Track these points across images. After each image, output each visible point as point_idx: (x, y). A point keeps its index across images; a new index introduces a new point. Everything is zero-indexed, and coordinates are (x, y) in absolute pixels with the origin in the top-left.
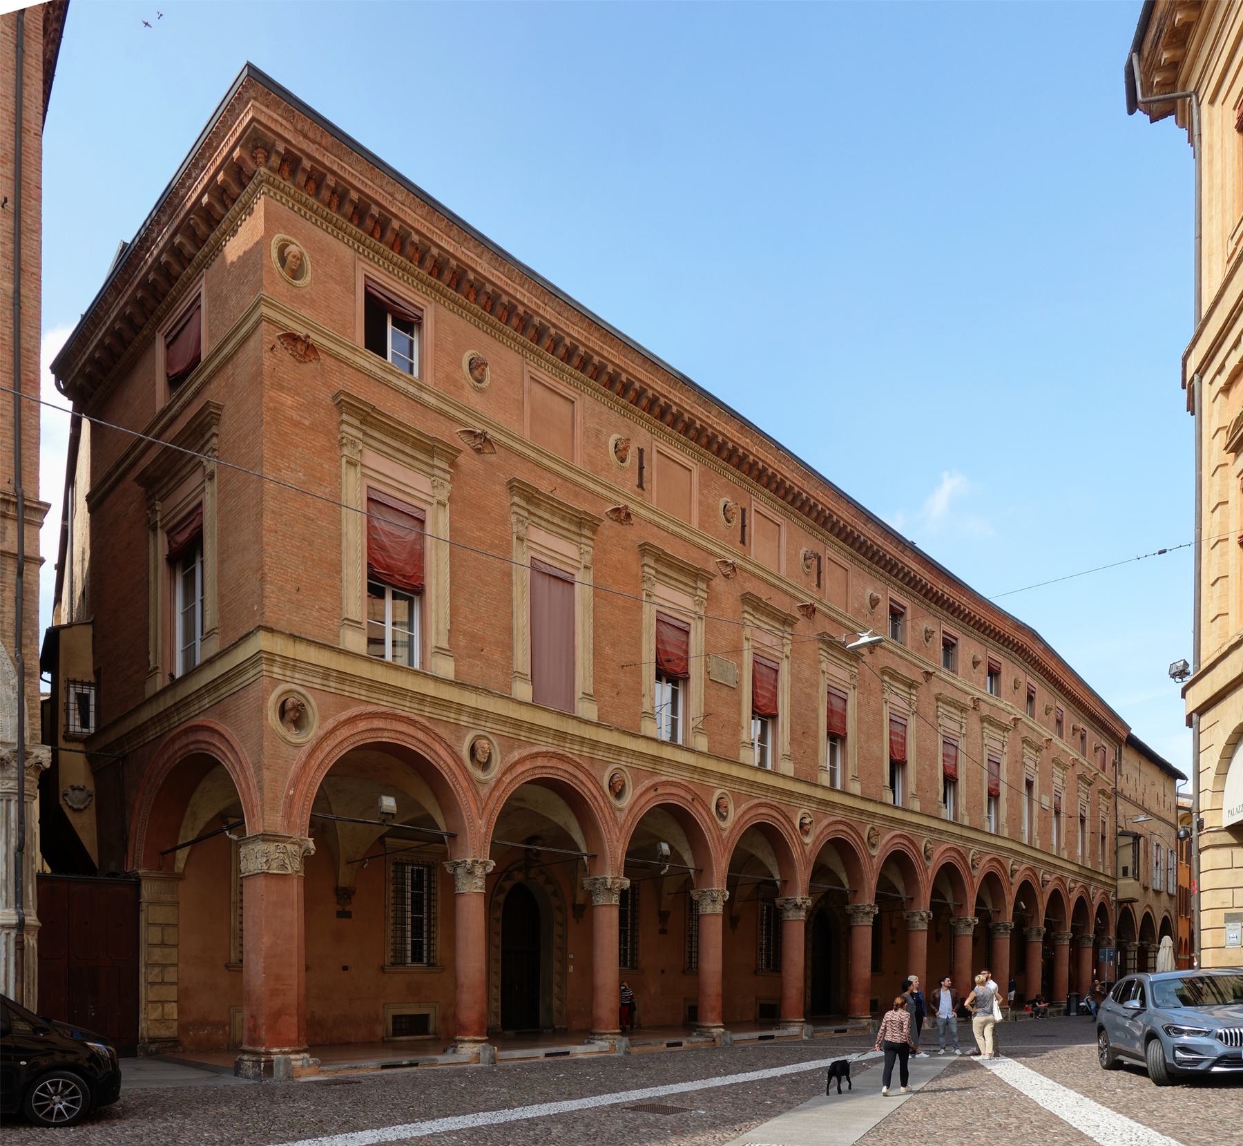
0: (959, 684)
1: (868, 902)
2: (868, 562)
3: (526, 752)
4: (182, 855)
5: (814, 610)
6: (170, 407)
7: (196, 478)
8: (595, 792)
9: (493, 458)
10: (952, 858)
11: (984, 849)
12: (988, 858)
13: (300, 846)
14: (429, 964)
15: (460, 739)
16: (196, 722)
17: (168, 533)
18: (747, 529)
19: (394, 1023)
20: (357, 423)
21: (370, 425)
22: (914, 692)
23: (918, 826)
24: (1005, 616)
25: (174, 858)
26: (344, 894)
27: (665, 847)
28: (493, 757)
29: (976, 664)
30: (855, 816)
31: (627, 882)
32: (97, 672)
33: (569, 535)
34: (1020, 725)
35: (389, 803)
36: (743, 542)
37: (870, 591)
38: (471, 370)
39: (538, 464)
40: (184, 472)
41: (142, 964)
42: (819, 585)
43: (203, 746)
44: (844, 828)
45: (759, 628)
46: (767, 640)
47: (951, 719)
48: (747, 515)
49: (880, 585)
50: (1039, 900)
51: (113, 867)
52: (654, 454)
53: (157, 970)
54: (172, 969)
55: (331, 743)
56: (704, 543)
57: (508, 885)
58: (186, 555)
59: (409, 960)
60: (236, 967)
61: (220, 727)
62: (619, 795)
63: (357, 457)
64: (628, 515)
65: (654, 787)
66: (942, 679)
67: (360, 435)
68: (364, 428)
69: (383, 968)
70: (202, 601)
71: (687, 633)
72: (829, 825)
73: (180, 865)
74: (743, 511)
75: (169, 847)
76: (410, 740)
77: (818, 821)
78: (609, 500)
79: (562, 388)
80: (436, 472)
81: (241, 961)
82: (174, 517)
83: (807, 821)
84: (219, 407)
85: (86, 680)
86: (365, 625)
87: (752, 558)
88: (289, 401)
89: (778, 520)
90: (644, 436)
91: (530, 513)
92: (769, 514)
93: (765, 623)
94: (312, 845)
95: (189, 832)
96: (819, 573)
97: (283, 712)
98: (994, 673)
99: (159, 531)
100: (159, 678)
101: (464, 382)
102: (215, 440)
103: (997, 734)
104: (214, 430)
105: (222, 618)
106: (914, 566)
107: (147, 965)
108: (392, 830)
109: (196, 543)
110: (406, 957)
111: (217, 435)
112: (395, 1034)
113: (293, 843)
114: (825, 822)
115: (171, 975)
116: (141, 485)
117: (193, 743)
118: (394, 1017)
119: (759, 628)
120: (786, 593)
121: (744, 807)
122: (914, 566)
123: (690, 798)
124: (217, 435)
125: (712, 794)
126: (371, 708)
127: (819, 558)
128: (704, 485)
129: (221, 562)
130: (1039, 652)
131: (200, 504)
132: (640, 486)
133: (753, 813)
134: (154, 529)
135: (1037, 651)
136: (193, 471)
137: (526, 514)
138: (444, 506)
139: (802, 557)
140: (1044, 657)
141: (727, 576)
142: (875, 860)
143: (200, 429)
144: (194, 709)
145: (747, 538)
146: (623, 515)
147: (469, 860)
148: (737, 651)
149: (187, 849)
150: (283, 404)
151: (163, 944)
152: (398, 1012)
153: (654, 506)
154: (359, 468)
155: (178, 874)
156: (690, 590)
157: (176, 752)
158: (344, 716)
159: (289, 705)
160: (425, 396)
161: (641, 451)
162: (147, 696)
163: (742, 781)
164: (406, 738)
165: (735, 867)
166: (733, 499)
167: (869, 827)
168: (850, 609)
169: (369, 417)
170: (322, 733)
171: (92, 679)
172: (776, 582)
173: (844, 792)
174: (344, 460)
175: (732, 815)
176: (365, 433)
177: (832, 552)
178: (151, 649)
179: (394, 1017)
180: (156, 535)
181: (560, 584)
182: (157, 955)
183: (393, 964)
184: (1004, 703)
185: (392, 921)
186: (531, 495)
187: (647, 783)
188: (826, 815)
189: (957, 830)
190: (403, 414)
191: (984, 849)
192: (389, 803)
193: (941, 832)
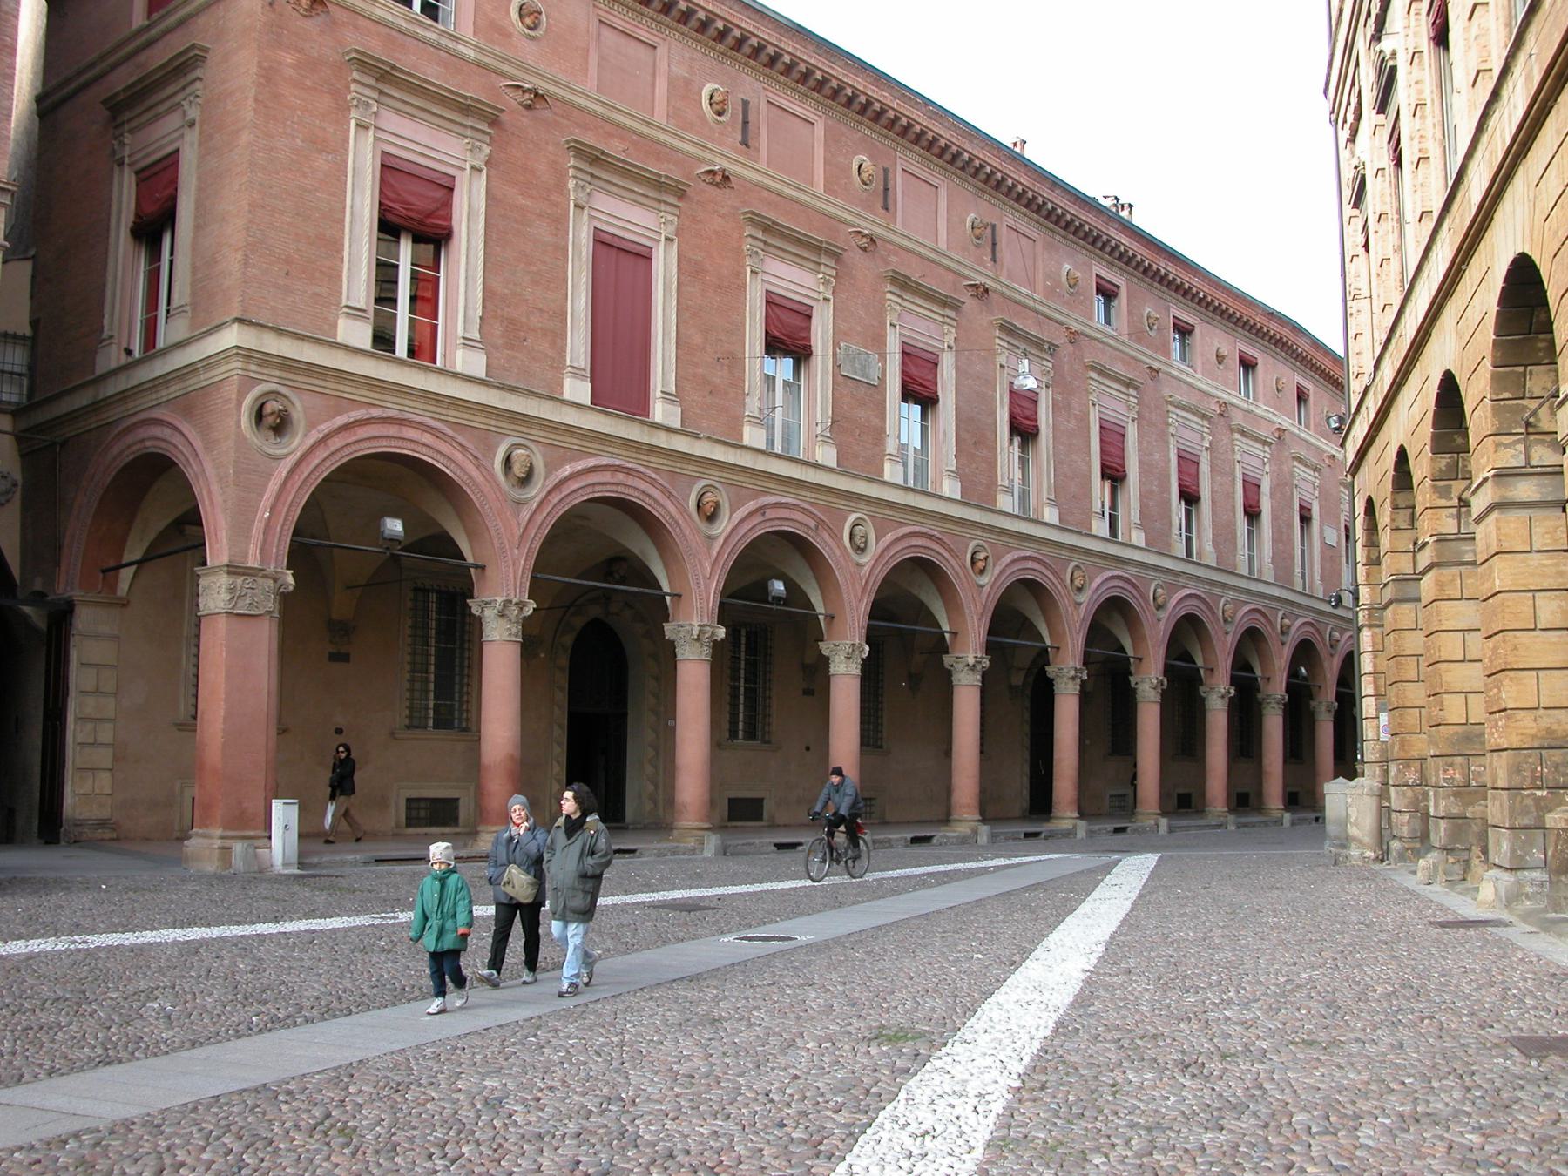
0: (1199, 384)
1: (1071, 664)
2: (1063, 232)
3: (580, 465)
4: (127, 574)
5: (986, 291)
6: (148, 28)
7: (173, 121)
8: (677, 516)
9: (547, 114)
10: (1193, 607)
11: (1243, 597)
12: (1247, 608)
13: (275, 580)
14: (764, 741)
15: (491, 450)
16: (156, 414)
17: (137, 173)
18: (890, 193)
19: (408, 808)
20: (371, 82)
21: (390, 83)
22: (1131, 391)
23: (1147, 566)
24: (1252, 303)
25: (117, 577)
26: (341, 630)
27: (779, 586)
28: (536, 472)
29: (1220, 359)
30: (1053, 551)
31: (721, 632)
32: (34, 323)
33: (645, 201)
34: (1286, 436)
35: (395, 526)
36: (886, 208)
37: (1067, 267)
38: (521, 16)
39: (606, 120)
40: (161, 108)
41: (70, 718)
42: (994, 260)
43: (163, 445)
44: (1037, 566)
45: (911, 311)
46: (922, 326)
47: (1191, 429)
48: (890, 176)
49: (1082, 258)
50: (1326, 664)
51: (38, 585)
52: (764, 106)
53: (90, 726)
54: (109, 726)
55: (322, 454)
56: (808, 199)
57: (579, 622)
58: (154, 228)
59: (431, 723)
60: (190, 723)
61: (185, 427)
62: (711, 518)
63: (370, 120)
64: (726, 178)
65: (761, 510)
66: (1174, 377)
67: (376, 95)
68: (380, 86)
69: (392, 734)
70: (171, 262)
71: (810, 317)
72: (1014, 561)
73: (123, 587)
74: (886, 171)
75: (112, 564)
76: (424, 450)
77: (998, 558)
78: (701, 161)
79: (642, 34)
80: (663, 207)
81: (195, 717)
82: (145, 157)
83: (981, 556)
84: (206, 50)
85: (20, 333)
86: (371, 315)
87: (899, 227)
88: (290, 59)
89: (935, 181)
90: (753, 87)
91: (765, 243)
92: (924, 175)
93: (917, 304)
94: (291, 580)
95: (134, 552)
96: (994, 244)
97: (259, 416)
98: (1247, 365)
99: (126, 169)
100: (114, 350)
101: (511, 29)
102: (198, 85)
103: (1256, 448)
104: (198, 73)
105: (193, 294)
106: (1124, 240)
107: (77, 719)
108: (394, 557)
109: (167, 218)
110: (426, 718)
111: (200, 79)
112: (408, 825)
113: (265, 576)
114: (1008, 558)
115: (106, 734)
116: (109, 109)
117: (150, 439)
118: (408, 800)
119: (911, 311)
120: (948, 269)
121: (890, 537)
122: (1124, 240)
123: (812, 524)
124: (200, 79)
125: (845, 519)
126: (375, 412)
127: (994, 227)
128: (831, 140)
129: (198, 228)
130: (1307, 348)
131: (177, 150)
132: (745, 143)
133: (904, 544)
134: (121, 163)
135: (1304, 346)
136: (171, 110)
137: (588, 178)
138: (480, 170)
139: (968, 224)
140: (1312, 352)
141: (864, 249)
142: (1083, 607)
143: (184, 66)
144: (153, 399)
145: (890, 202)
146: (718, 178)
147: (500, 599)
148: (878, 342)
149: (134, 568)
150: (280, 63)
151: (97, 692)
152: (415, 794)
153: (762, 166)
154: (371, 132)
155: (120, 598)
156: (812, 266)
157: (129, 447)
158: (341, 420)
159: (268, 409)
160: (461, 48)
161: (745, 104)
162: (98, 372)
163: (891, 505)
164: (419, 448)
165: (879, 610)
166: (871, 157)
167: (1072, 565)
168: (1039, 286)
169: (385, 76)
170: (310, 442)
171: (28, 332)
172: (932, 256)
173: (1038, 522)
174: (353, 123)
175: (874, 548)
176: (381, 92)
177: (1009, 219)
178: (107, 310)
179: (408, 800)
180: (122, 172)
181: (632, 257)
182: (90, 706)
183: (408, 727)
184: (1262, 409)
185: (408, 667)
186: (593, 158)
187: (751, 505)
188: (1010, 550)
189: (1190, 569)
190: (433, 73)
191: (1243, 597)
192: (395, 526)
193: (1177, 574)
